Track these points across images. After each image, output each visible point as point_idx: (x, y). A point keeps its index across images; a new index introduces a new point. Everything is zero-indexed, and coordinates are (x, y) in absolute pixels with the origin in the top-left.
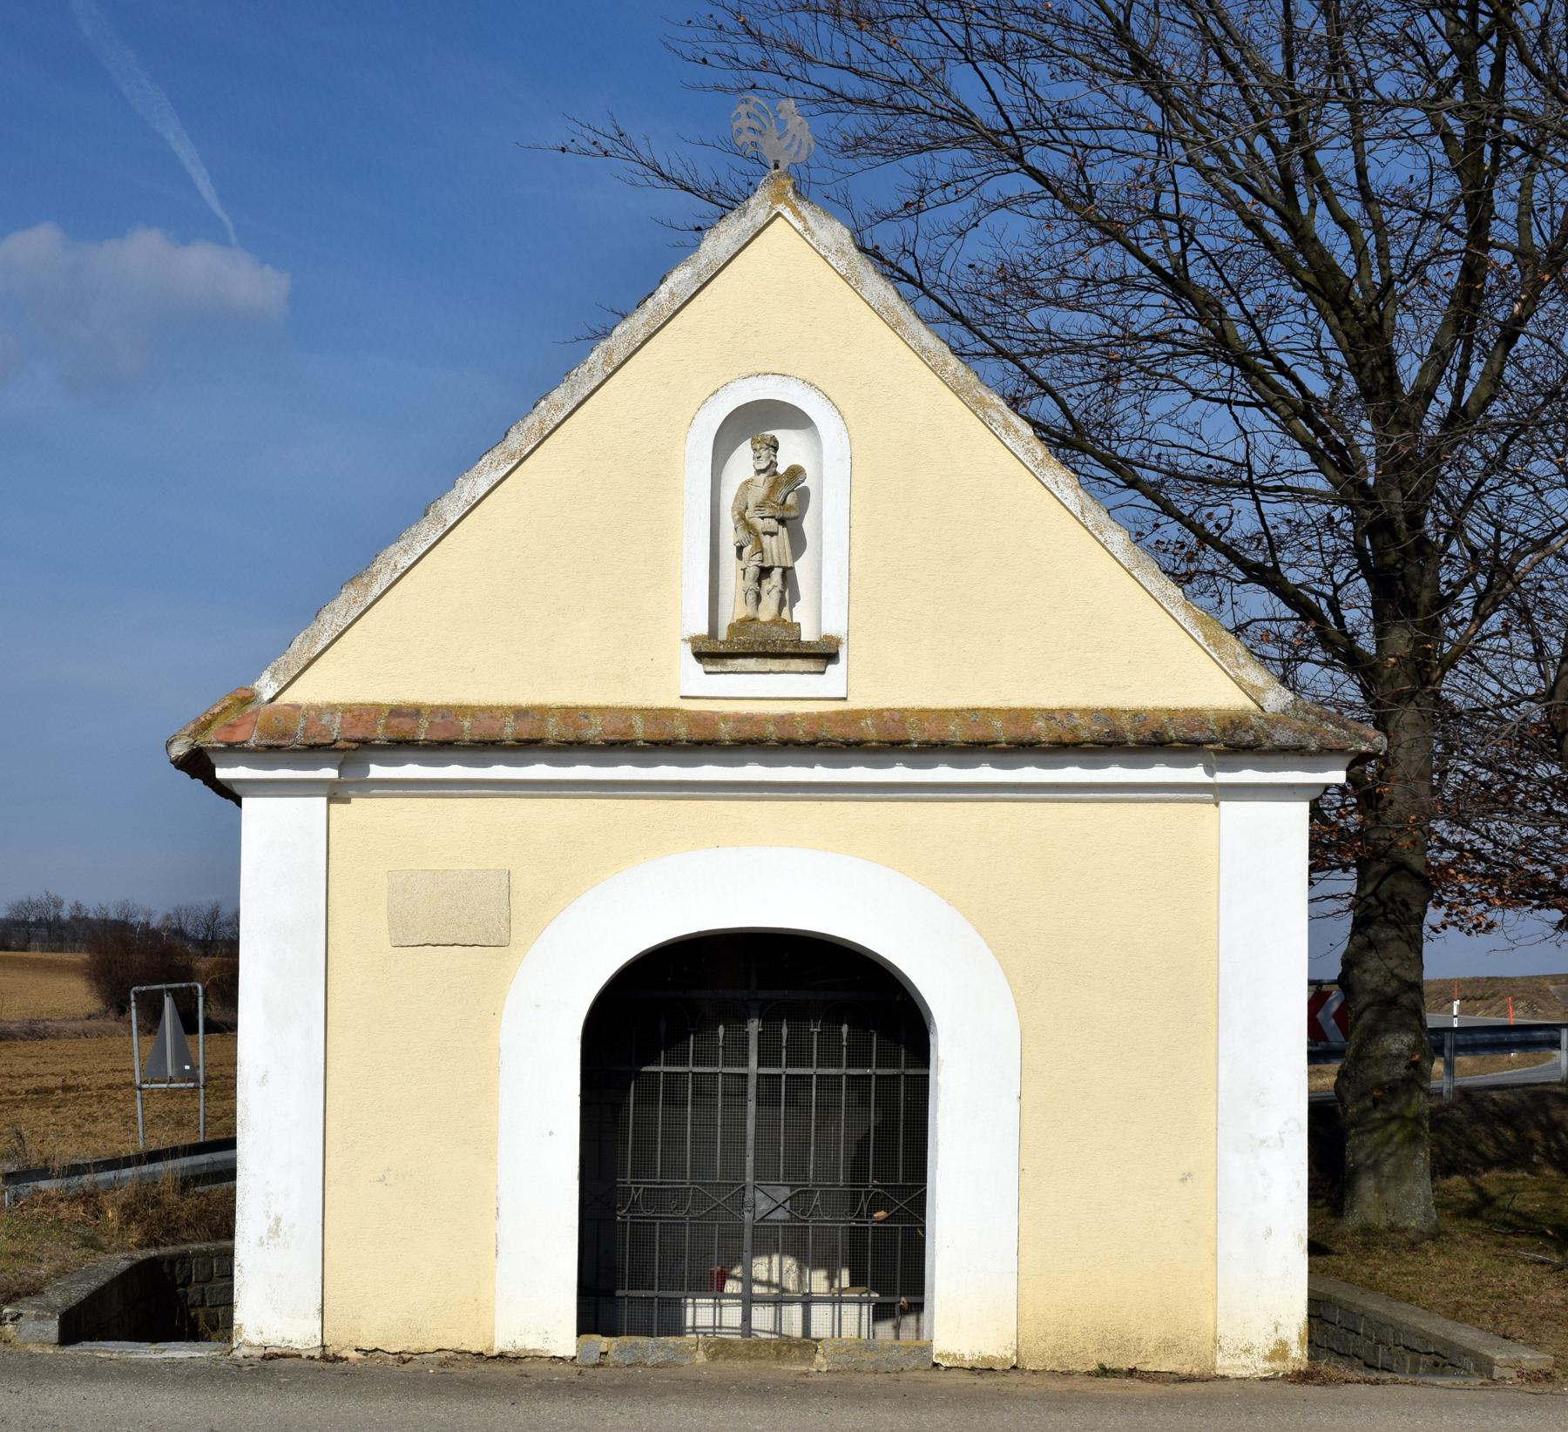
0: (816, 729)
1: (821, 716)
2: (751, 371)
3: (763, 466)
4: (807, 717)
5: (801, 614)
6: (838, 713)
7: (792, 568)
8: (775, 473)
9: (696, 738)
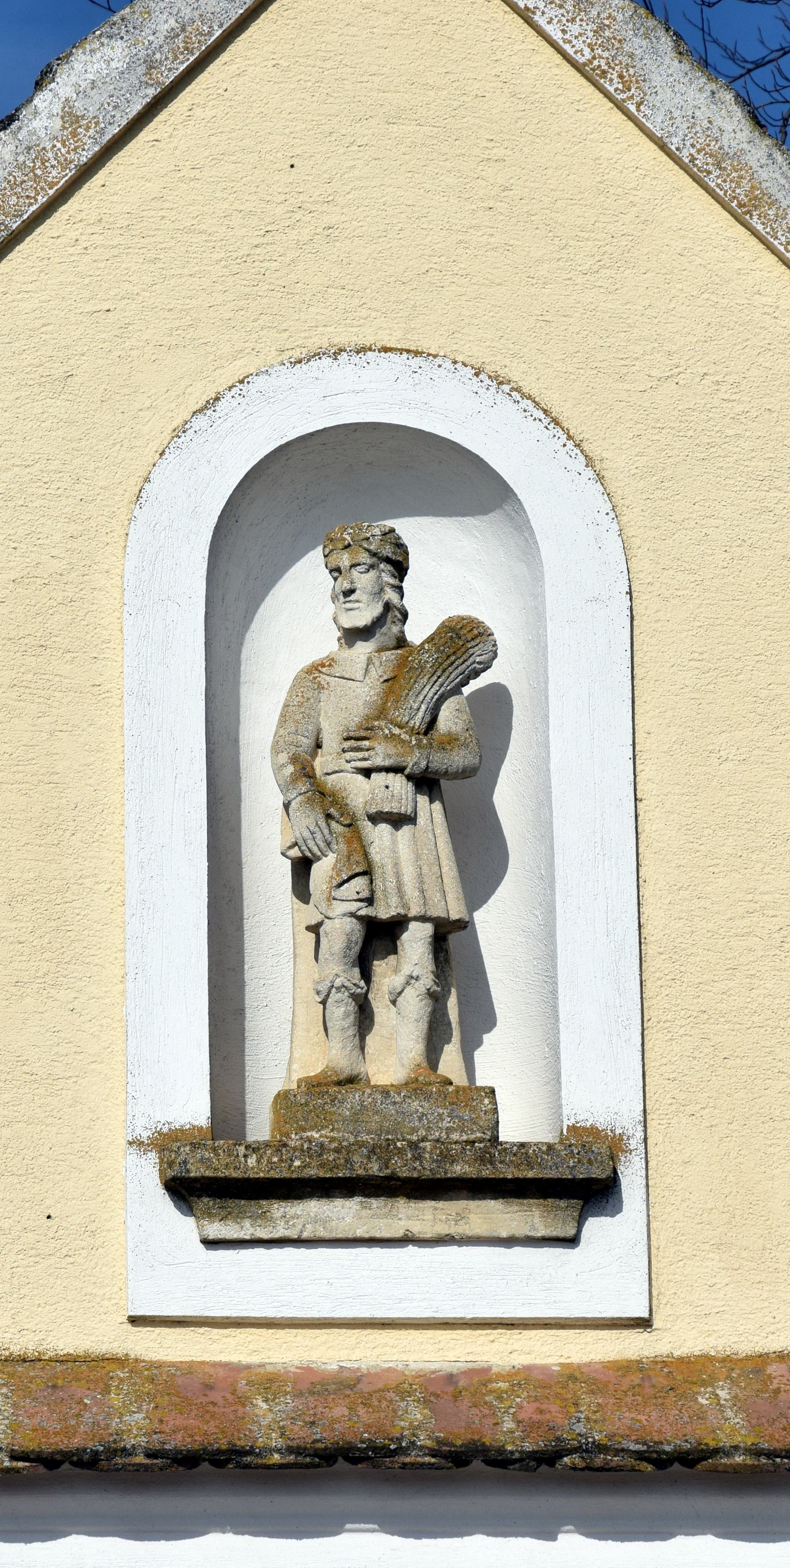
0: (554, 1412)
1: (572, 1375)
2: (317, 341)
3: (363, 617)
4: (525, 1378)
5: (501, 1063)
6: (626, 1367)
7: (463, 925)
8: (401, 642)
9: (177, 1442)
